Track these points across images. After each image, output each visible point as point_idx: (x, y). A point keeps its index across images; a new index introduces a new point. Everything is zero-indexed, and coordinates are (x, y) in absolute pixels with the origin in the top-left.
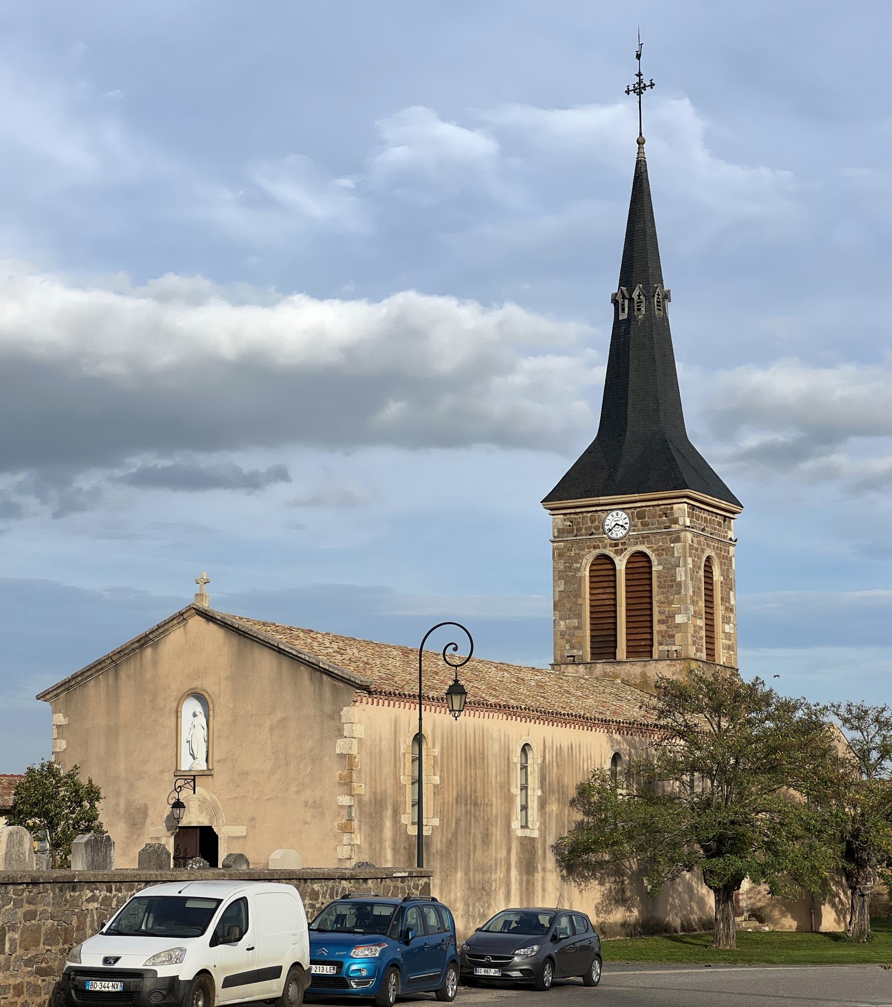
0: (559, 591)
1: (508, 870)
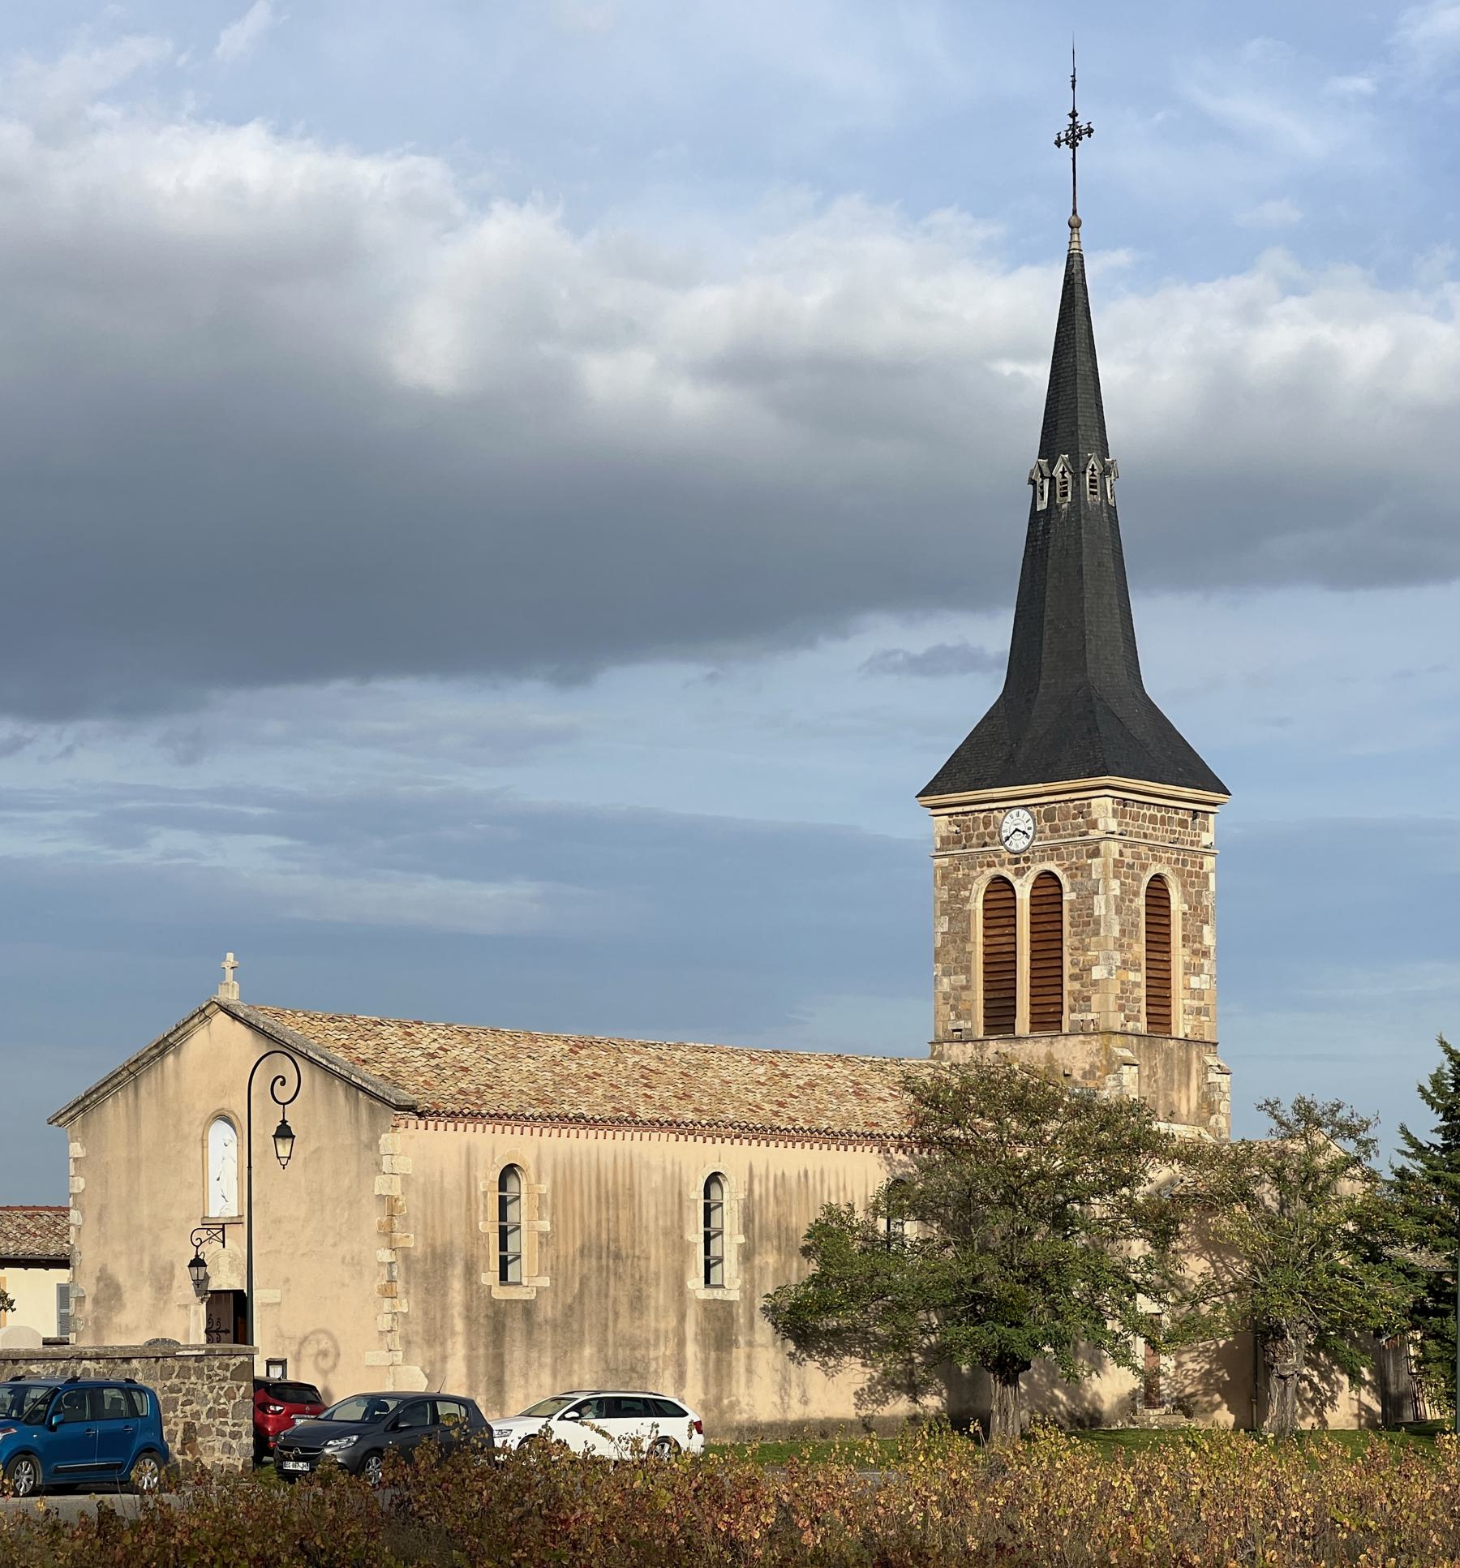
0: (942, 933)
1: (681, 1343)
